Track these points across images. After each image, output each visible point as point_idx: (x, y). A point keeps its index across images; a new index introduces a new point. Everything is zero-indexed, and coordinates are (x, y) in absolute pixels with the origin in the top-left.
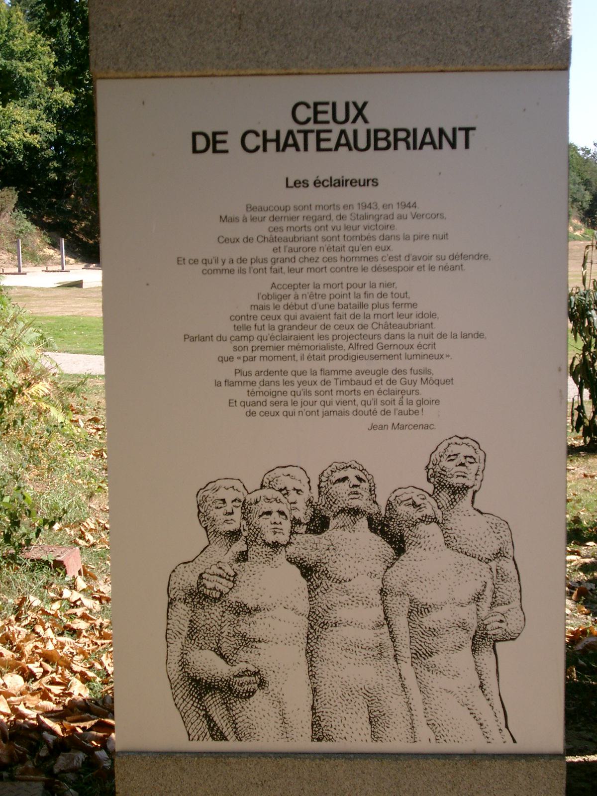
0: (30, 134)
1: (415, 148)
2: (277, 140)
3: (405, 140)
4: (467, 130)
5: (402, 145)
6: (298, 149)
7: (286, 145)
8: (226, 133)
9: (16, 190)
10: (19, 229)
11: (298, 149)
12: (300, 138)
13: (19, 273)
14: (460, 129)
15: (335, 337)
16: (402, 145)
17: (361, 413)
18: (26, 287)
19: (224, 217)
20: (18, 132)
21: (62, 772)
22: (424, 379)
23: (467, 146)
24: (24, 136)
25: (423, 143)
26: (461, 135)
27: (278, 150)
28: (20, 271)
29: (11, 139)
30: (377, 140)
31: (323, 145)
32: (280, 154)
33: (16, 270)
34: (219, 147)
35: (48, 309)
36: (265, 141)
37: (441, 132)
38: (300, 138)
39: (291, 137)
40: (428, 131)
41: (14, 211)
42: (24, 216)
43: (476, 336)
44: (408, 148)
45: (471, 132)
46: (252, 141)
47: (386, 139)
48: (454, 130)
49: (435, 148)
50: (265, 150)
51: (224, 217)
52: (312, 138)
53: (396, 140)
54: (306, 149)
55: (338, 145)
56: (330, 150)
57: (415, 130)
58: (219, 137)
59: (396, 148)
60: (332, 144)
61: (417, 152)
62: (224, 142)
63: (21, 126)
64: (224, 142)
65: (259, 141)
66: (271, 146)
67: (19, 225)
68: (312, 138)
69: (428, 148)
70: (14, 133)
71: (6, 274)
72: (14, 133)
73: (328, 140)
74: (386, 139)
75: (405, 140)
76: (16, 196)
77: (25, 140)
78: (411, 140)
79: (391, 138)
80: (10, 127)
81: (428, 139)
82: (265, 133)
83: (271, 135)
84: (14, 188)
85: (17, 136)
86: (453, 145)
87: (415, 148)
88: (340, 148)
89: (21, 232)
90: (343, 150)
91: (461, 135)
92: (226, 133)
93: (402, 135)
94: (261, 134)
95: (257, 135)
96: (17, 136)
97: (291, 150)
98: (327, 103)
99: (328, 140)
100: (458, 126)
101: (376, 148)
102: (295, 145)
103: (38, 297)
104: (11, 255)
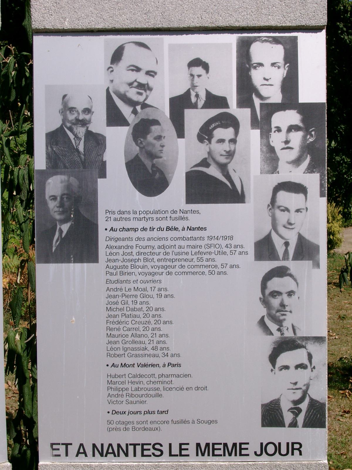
3: (298, 449)
4: (67, 445)
14: (130, 444)
15: (111, 429)
17: (150, 396)
19: (136, 288)
25: (107, 453)
26: (131, 448)
34: (243, 452)
37: (119, 446)
40: (110, 445)
45: (69, 446)
48: (127, 445)
49: (115, 456)
51: (136, 288)
52: (139, 448)
53: (293, 449)
56: (221, 455)
58: (243, 446)
59: (293, 454)
62: (187, 449)
64: (247, 449)
68: (139, 448)
75: (298, 449)
91: (131, 448)
98: (150, 444)
100: (129, 443)
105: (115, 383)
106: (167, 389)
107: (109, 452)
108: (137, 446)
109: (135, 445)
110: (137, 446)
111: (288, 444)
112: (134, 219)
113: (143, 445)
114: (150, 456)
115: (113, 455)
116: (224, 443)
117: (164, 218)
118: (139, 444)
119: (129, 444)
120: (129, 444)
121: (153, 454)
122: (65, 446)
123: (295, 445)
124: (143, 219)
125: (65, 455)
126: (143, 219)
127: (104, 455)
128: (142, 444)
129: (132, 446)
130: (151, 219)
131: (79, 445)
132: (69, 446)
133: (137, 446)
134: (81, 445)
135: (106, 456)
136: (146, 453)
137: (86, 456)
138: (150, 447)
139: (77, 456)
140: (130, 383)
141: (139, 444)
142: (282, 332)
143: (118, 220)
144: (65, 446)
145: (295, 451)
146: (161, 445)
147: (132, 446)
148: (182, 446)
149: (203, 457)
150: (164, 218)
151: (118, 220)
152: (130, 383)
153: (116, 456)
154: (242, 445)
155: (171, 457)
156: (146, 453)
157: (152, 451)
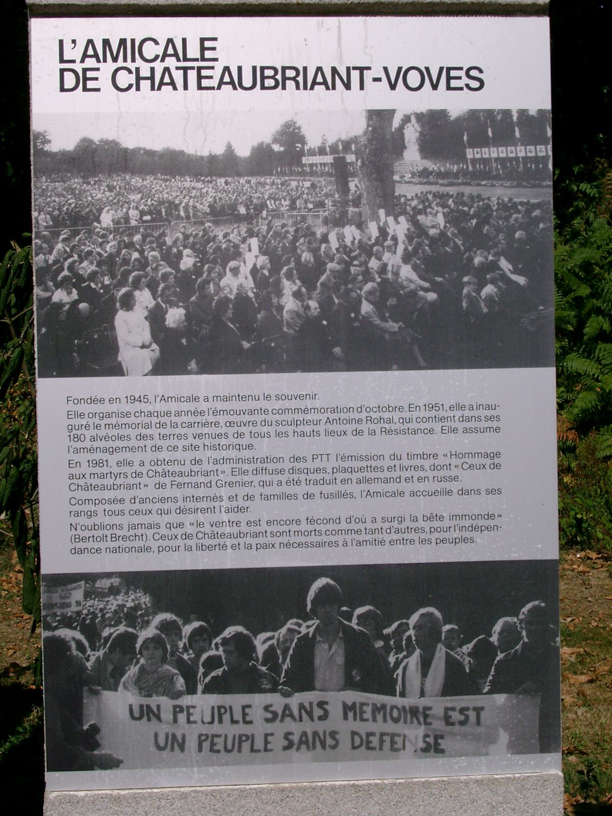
3: (294, 79)
5: (290, 84)
8: (215, 39)
14: (355, 68)
16: (290, 84)
26: (355, 75)
34: (90, 84)
36: (139, 79)
37: (334, 71)
39: (167, 75)
40: (319, 69)
44: (298, 88)
48: (348, 69)
49: (328, 88)
50: (138, 89)
56: (213, 88)
62: (96, 79)
64: (96, 79)
75: (294, 79)
91: (355, 75)
92: (215, 39)
98: (461, 69)
105: (109, 415)
106: (295, 545)
108: (189, 72)
110: (189, 72)
111: (254, 68)
114: (461, 89)
115: (171, 87)
121: (467, 86)
122: (182, 71)
123: (287, 71)
127: (309, 87)
129: (358, 72)
133: (365, 71)
136: (454, 83)
137: (175, 88)
138: (462, 73)
140: (453, 457)
142: (233, 207)
145: (287, 81)
146: (481, 71)
147: (358, 72)
148: (451, 71)
149: (393, 91)
152: (453, 457)
154: (88, 73)
156: (454, 83)
157: (465, 80)
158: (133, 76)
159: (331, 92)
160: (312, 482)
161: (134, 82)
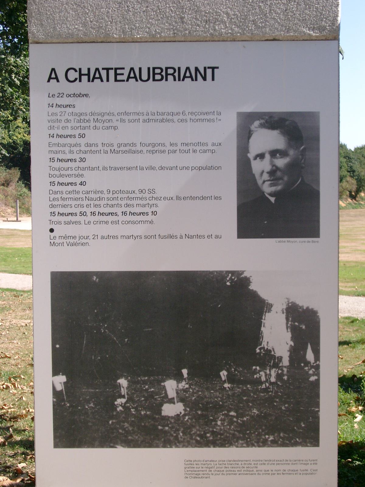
0: (28, 135)
1: (179, 80)
2: (88, 75)
4: (213, 68)
5: (170, 78)
6: (102, 81)
7: (94, 77)
9: (19, 169)
10: (19, 193)
11: (102, 81)
12: (104, 73)
13: (17, 221)
14: (209, 68)
16: (170, 78)
18: (15, 230)
20: (20, 134)
21: (282, 366)
22: (52, 243)
23: (213, 79)
24: (24, 136)
25: (185, 77)
26: (209, 72)
27: (89, 81)
28: (17, 219)
29: (15, 138)
30: (154, 74)
31: (119, 78)
32: (91, 83)
33: (15, 219)
35: (17, 243)
36: (81, 75)
37: (197, 69)
38: (104, 73)
40: (188, 68)
41: (18, 182)
42: (23, 185)
43: (201, 198)
44: (175, 80)
45: (215, 70)
46: (72, 75)
47: (160, 74)
48: (205, 68)
49: (192, 80)
50: (80, 81)
52: (112, 73)
53: (167, 74)
54: (108, 80)
55: (129, 77)
56: (124, 81)
57: (179, 68)
58: (119, 71)
59: (167, 80)
60: (125, 77)
61: (181, 82)
63: (22, 130)
65: (77, 75)
66: (85, 78)
67: (20, 191)
68: (112, 73)
69: (188, 80)
70: (17, 134)
71: (9, 221)
72: (17, 134)
73: (123, 74)
74: (160, 74)
76: (19, 173)
77: (24, 138)
78: (176, 74)
79: (164, 74)
80: (14, 131)
81: (188, 74)
82: (80, 69)
83: (84, 71)
84: (18, 168)
85: (19, 136)
86: (204, 79)
87: (179, 80)
88: (130, 80)
89: (21, 195)
90: (132, 81)
91: (209, 72)
93: (170, 71)
94: (78, 70)
95: (76, 71)
96: (19, 136)
97: (97, 81)
99: (123, 74)
101: (154, 80)
102: (100, 78)
103: (19, 235)
104: (14, 209)
107: (96, 76)
108: (110, 71)
109: (108, 70)
110: (110, 71)
111: (149, 69)
112: (122, 237)
113: (116, 69)
116: (115, 68)
117: (153, 237)
118: (112, 69)
119: (207, 68)
120: (207, 68)
122: (211, 69)
124: (131, 237)
125: (211, 80)
126: (131, 237)
127: (91, 81)
128: (115, 68)
129: (211, 70)
130: (139, 237)
131: (95, 70)
132: (215, 70)
133: (215, 69)
134: (53, 70)
135: (183, 80)
139: (49, 81)
141: (112, 69)
143: (106, 238)
144: (211, 69)
150: (153, 237)
151: (106, 238)
153: (193, 81)
155: (154, 82)
158: (78, 73)
159: (194, 82)
160: (113, 168)
161: (78, 76)
